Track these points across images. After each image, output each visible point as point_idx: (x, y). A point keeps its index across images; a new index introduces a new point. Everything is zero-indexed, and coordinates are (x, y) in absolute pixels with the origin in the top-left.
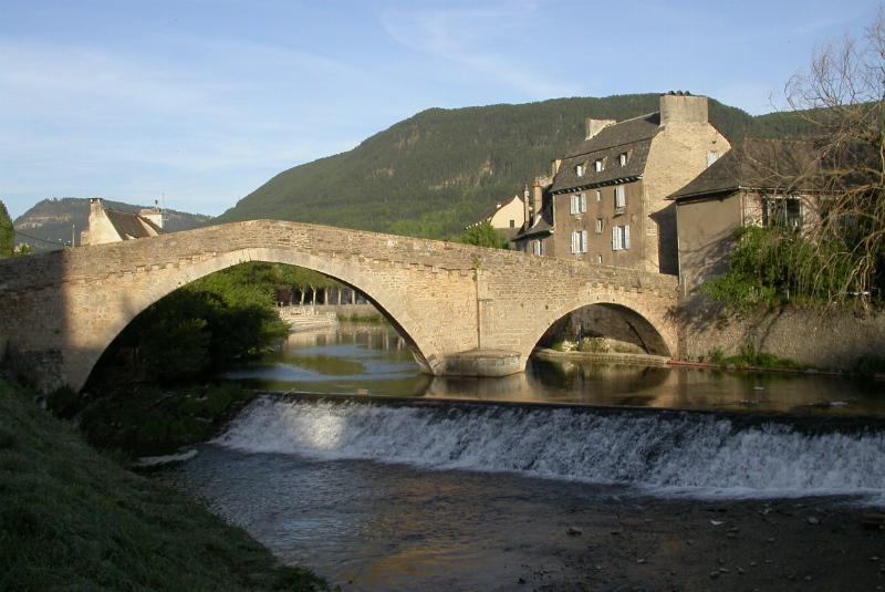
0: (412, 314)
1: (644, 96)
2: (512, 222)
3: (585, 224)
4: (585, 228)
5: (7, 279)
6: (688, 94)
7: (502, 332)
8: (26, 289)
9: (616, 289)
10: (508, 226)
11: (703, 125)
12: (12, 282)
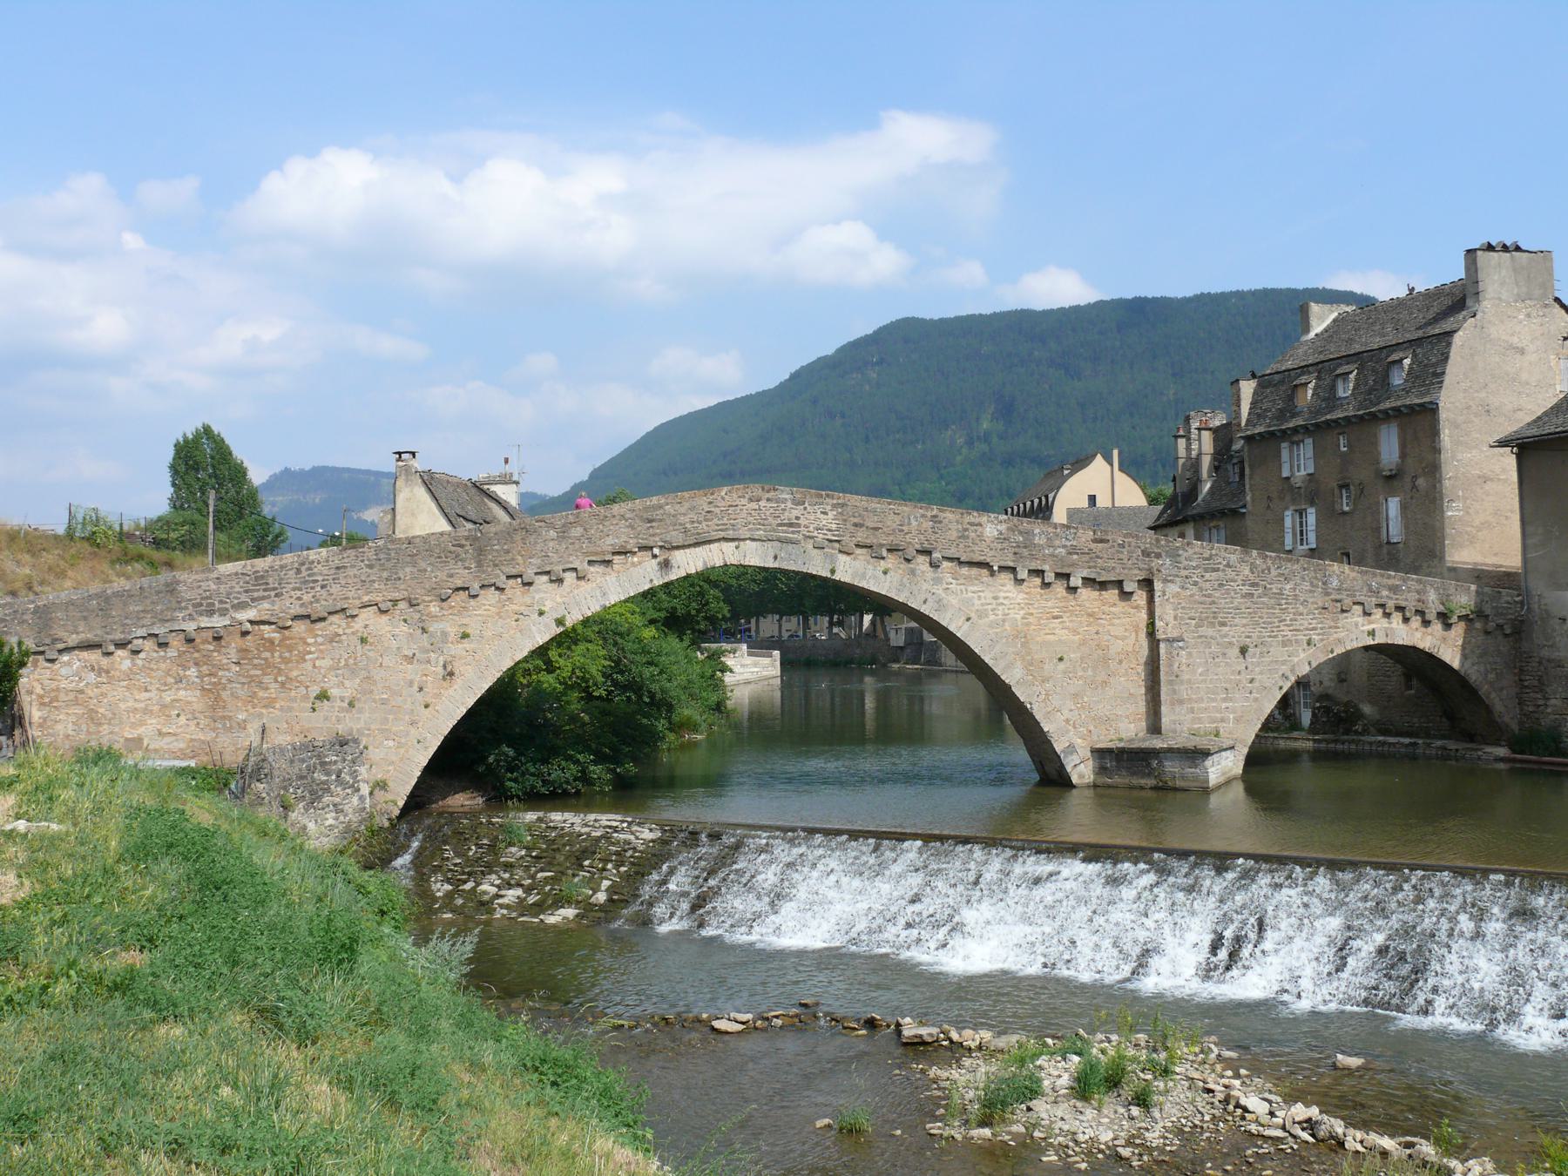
0: (1031, 665)
1: (1254, 293)
2: (1092, 499)
3: (1311, 493)
4: (1312, 504)
5: (253, 600)
6: (1518, 249)
7: (1201, 700)
8: (296, 618)
9: (1406, 620)
10: (1086, 504)
11: (1546, 306)
12: (266, 605)
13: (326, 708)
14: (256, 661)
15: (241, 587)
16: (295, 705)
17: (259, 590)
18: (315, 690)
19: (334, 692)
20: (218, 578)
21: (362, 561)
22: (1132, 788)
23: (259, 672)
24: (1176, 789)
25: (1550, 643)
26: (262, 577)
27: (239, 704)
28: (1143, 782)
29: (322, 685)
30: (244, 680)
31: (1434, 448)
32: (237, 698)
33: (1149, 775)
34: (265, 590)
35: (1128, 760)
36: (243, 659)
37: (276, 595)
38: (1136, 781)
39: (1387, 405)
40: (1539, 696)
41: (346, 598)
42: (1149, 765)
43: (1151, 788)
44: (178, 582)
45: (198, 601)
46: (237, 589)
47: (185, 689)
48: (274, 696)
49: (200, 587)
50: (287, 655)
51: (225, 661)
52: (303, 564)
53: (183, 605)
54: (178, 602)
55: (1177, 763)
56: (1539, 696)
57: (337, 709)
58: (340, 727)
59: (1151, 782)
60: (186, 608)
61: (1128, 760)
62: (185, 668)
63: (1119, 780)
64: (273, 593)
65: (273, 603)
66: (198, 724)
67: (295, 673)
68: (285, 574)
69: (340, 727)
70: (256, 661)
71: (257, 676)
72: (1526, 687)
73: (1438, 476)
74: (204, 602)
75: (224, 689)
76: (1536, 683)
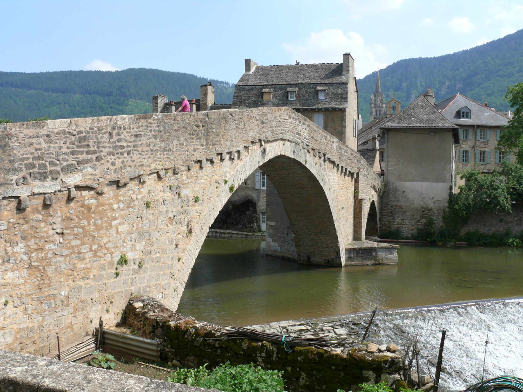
13: (124, 271)
14: (76, 230)
15: (68, 148)
16: (104, 273)
17: (82, 153)
18: (117, 257)
19: (130, 256)
20: (48, 136)
21: (151, 131)
22: (363, 265)
23: (78, 242)
24: (383, 264)
25: (397, 200)
26: (85, 138)
27: (62, 280)
28: (368, 262)
29: (122, 250)
30: (66, 252)
31: (342, 125)
32: (60, 273)
33: (371, 259)
34: (88, 153)
35: (362, 253)
36: (66, 229)
37: (97, 159)
38: (365, 262)
39: (316, 107)
40: (391, 218)
41: (142, 165)
42: (371, 254)
43: (372, 265)
44: (9, 136)
45: (30, 161)
46: (64, 150)
47: (13, 270)
48: (89, 266)
49: (31, 144)
50: (99, 222)
51: (51, 232)
52: (114, 128)
53: (16, 164)
54: (11, 162)
55: (384, 253)
56: (391, 218)
57: (131, 272)
58: (133, 288)
59: (372, 262)
60: (20, 170)
61: (362, 253)
62: (13, 243)
63: (357, 262)
64: (94, 157)
65: (94, 168)
66: (26, 309)
67: (105, 240)
68: (101, 138)
69: (133, 288)
70: (76, 230)
71: (77, 246)
72: (384, 215)
73: (343, 136)
74: (36, 163)
75: (49, 264)
76: (390, 214)
